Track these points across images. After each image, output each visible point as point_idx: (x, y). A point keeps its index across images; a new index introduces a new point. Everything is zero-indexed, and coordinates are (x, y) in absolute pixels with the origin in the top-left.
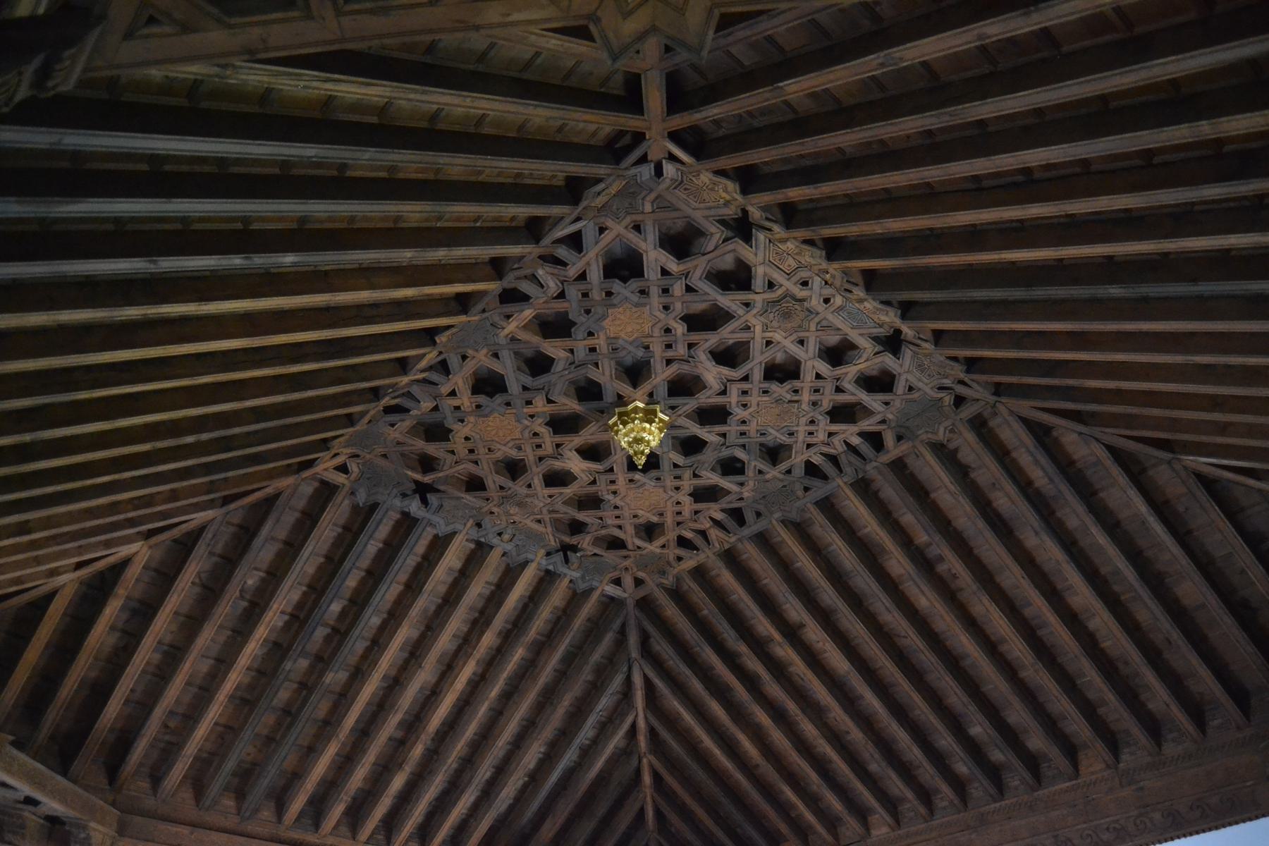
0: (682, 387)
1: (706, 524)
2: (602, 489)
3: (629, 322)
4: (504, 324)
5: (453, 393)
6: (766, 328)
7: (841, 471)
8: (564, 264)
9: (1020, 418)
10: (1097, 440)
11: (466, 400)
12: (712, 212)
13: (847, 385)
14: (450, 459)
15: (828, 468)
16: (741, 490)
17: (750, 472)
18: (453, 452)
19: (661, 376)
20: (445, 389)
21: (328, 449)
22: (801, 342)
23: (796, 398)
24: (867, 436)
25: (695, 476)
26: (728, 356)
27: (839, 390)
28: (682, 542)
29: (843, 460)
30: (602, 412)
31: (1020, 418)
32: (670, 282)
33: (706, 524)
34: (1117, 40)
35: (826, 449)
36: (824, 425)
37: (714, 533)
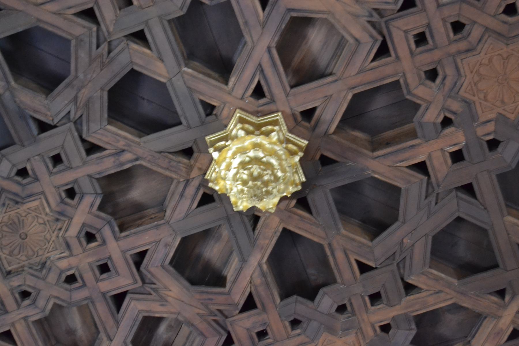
10: (64, 141)
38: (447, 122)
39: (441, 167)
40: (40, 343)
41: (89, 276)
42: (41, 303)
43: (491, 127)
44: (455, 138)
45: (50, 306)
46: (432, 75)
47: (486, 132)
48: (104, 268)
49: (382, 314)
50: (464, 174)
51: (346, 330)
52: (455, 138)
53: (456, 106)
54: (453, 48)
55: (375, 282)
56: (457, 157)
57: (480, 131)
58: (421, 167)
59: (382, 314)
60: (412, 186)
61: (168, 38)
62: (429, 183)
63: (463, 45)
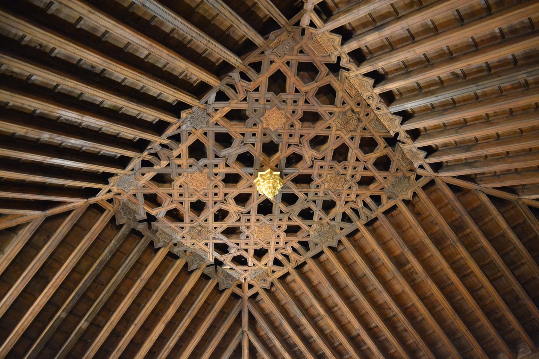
0: (294, 159)
1: (289, 251)
2: (242, 225)
3: (274, 119)
4: (214, 114)
5: (179, 156)
6: (338, 130)
7: (359, 218)
8: (249, 80)
9: (249, 340)
10: (483, 192)
11: (185, 160)
12: (324, 59)
13: (370, 166)
14: (169, 199)
15: (353, 216)
16: (311, 231)
17: (316, 218)
18: (171, 195)
19: (282, 155)
20: (175, 153)
21: (107, 183)
22: (206, 244)
23: (345, 173)
24: (373, 197)
25: (290, 219)
26: (242, 199)
27: (365, 168)
28: (277, 262)
29: (361, 212)
30: (251, 175)
31: (249, 340)
32: (298, 97)
33: (289, 251)
34: (462, 20)
35: (354, 206)
36: (356, 189)
37: (293, 256)
38: (216, 175)
39: (222, 165)
40: (537, 68)
41: (320, 171)
42: (343, 165)
43: (205, 171)
44: (216, 170)
45: (341, 163)
46: (216, 186)
47: (206, 170)
48: (322, 167)
49: (253, 220)
50: (216, 161)
51: (272, 108)
52: (216, 170)
53: (213, 178)
54: (208, 191)
55: (252, 140)
56: (216, 166)
57: (208, 170)
58: (227, 165)
59: (253, 220)
60: (231, 162)
61: (33, 68)
62: (227, 161)
63: (206, 191)
